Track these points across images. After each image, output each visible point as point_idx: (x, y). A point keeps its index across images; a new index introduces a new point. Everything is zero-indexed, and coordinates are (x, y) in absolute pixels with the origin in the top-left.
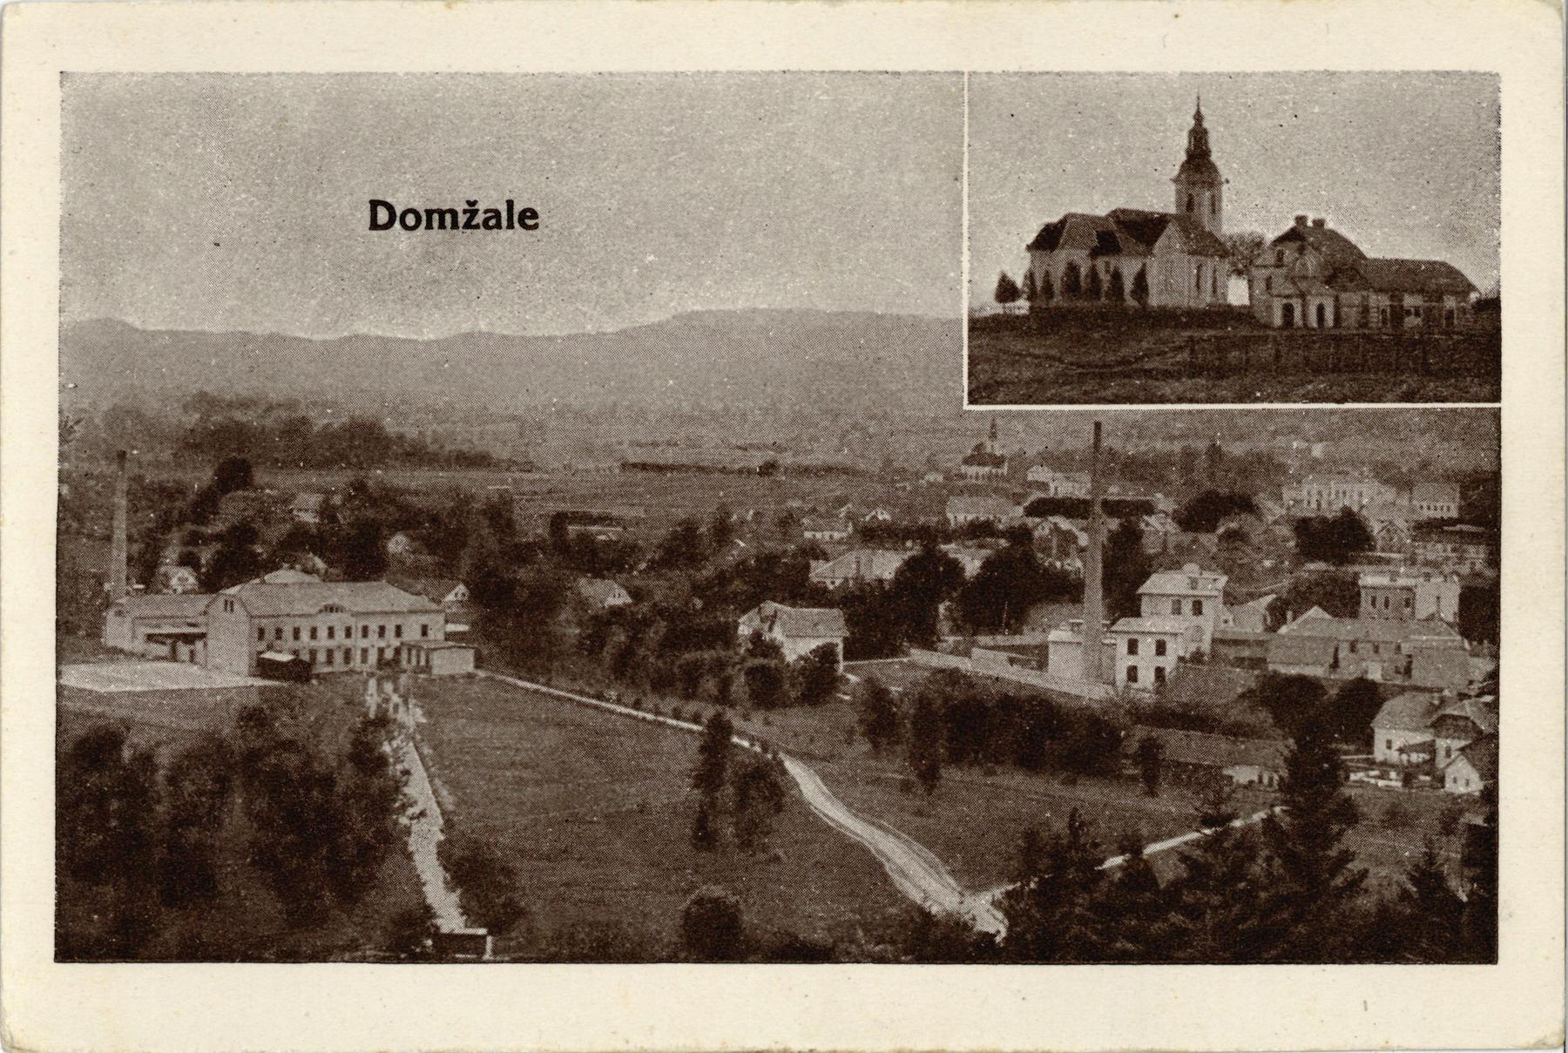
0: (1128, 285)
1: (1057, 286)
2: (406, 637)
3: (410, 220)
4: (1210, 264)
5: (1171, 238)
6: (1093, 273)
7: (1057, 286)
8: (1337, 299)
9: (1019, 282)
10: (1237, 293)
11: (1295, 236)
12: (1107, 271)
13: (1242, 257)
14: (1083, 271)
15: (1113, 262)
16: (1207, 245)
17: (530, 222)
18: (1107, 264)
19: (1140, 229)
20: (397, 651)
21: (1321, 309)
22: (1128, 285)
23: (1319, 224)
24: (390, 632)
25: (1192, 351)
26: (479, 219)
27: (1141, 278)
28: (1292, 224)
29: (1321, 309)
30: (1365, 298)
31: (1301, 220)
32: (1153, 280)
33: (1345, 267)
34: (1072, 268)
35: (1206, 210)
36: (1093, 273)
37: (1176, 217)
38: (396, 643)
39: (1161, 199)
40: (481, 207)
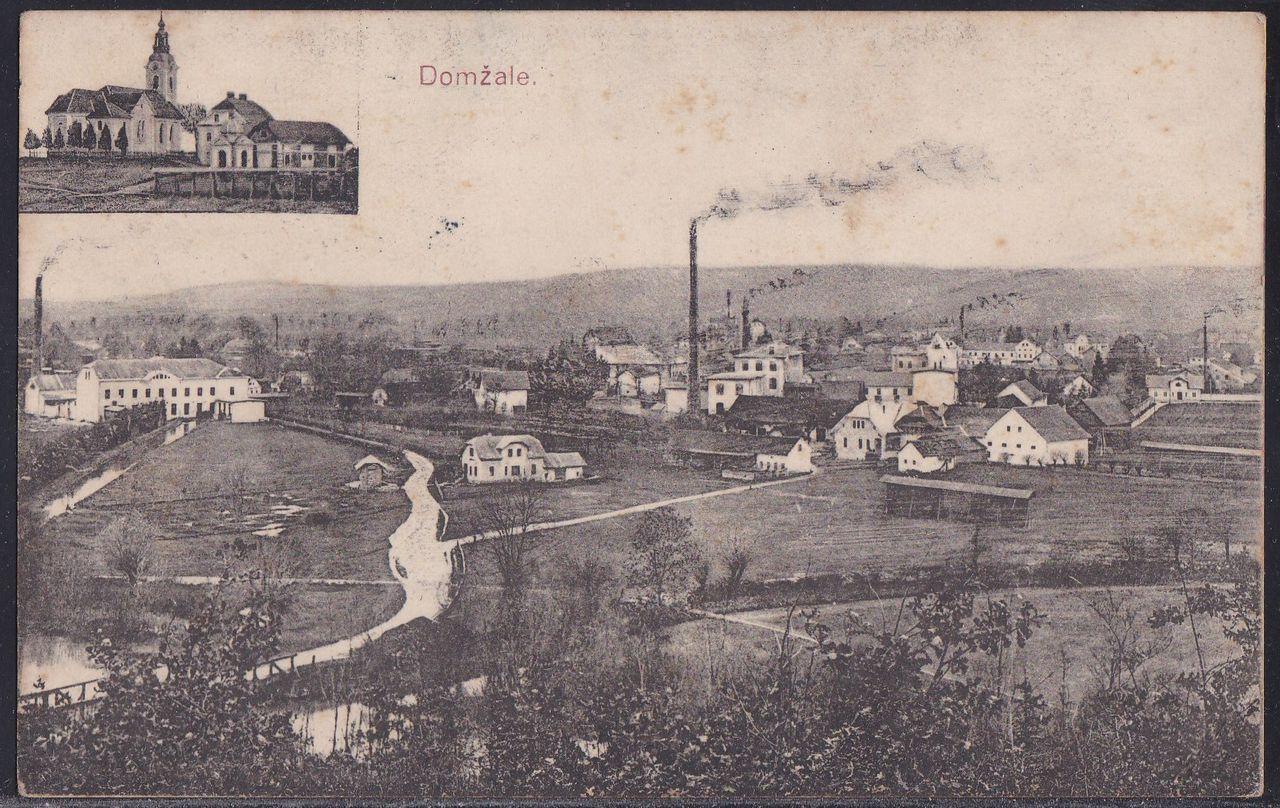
0: (115, 136)
1: (66, 137)
2: (218, 395)
3: (446, 79)
4: (169, 123)
5: (144, 109)
6: (90, 127)
7: (66, 137)
8: (255, 148)
9: (40, 137)
10: (187, 143)
11: (227, 105)
12: (100, 128)
13: (191, 117)
14: (84, 127)
15: (104, 121)
16: (167, 111)
17: (523, 81)
18: (100, 123)
19: (121, 100)
20: (212, 405)
21: (244, 154)
22: (115, 136)
23: (243, 97)
24: (206, 392)
25: (157, 181)
26: (491, 79)
27: (122, 132)
28: (224, 97)
29: (244, 154)
30: (275, 147)
31: (231, 95)
32: (131, 135)
33: (264, 128)
34: (77, 126)
35: (166, 86)
36: (90, 127)
37: (146, 92)
38: (212, 399)
39: (137, 80)
40: (493, 70)
